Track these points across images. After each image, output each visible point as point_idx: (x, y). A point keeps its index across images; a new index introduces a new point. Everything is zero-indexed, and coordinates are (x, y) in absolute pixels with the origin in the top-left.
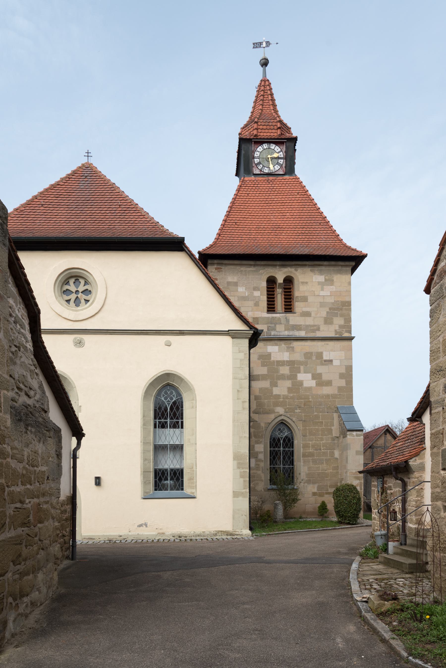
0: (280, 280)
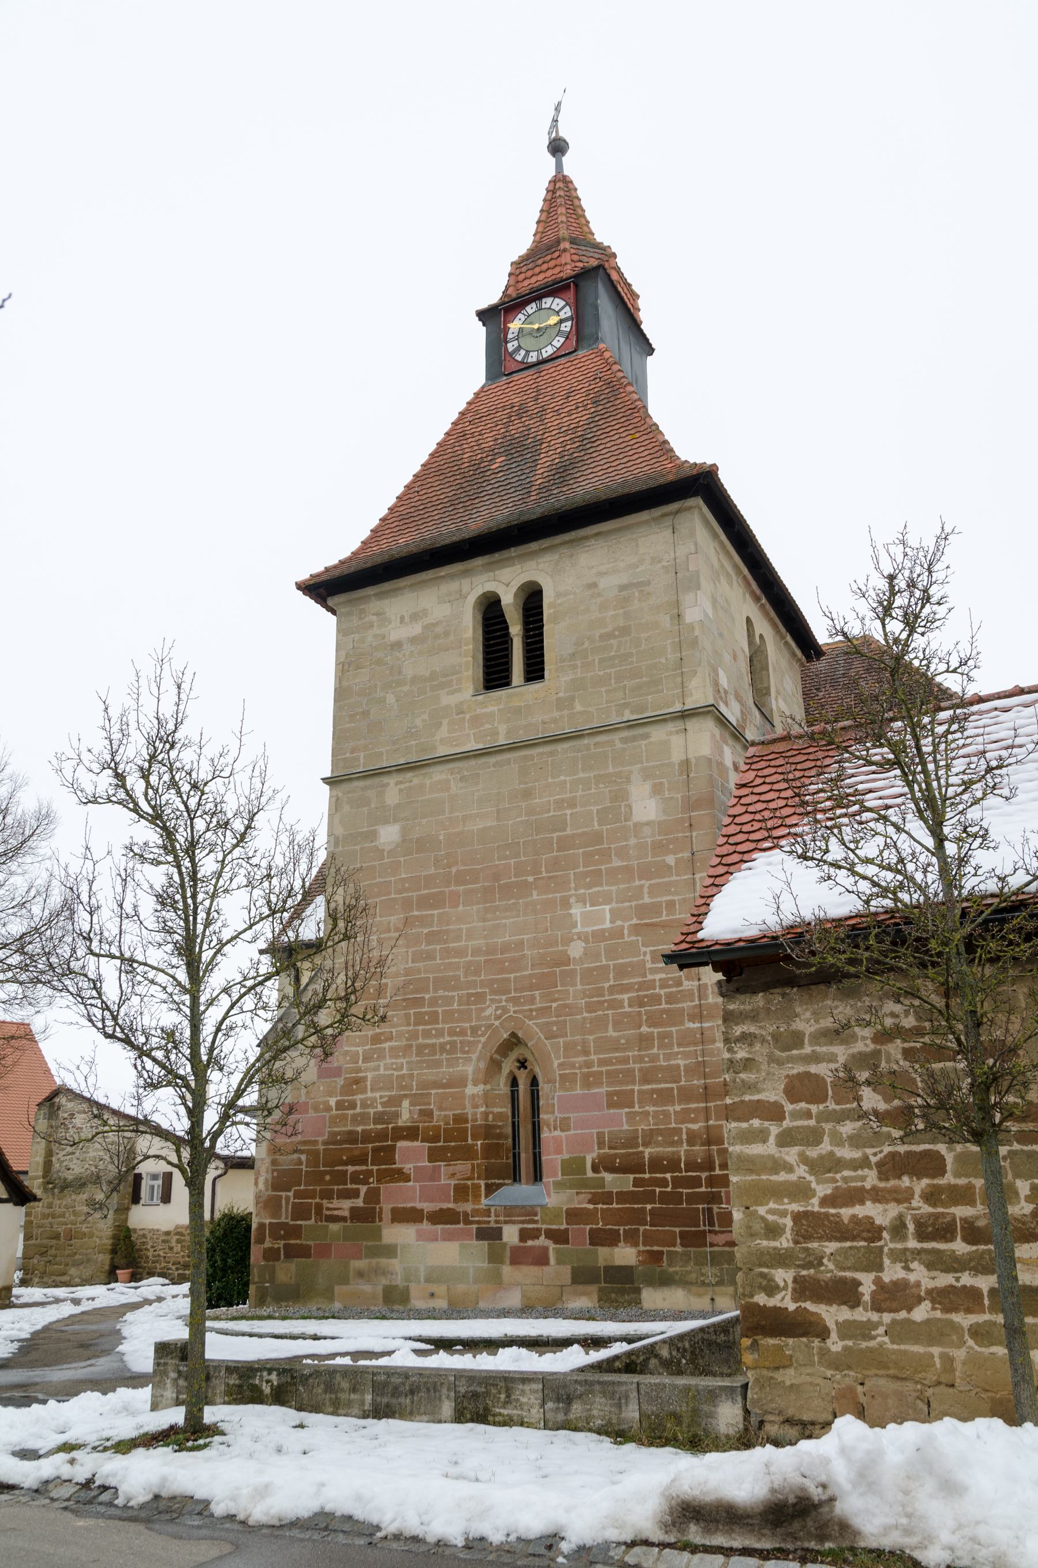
0: (508, 599)
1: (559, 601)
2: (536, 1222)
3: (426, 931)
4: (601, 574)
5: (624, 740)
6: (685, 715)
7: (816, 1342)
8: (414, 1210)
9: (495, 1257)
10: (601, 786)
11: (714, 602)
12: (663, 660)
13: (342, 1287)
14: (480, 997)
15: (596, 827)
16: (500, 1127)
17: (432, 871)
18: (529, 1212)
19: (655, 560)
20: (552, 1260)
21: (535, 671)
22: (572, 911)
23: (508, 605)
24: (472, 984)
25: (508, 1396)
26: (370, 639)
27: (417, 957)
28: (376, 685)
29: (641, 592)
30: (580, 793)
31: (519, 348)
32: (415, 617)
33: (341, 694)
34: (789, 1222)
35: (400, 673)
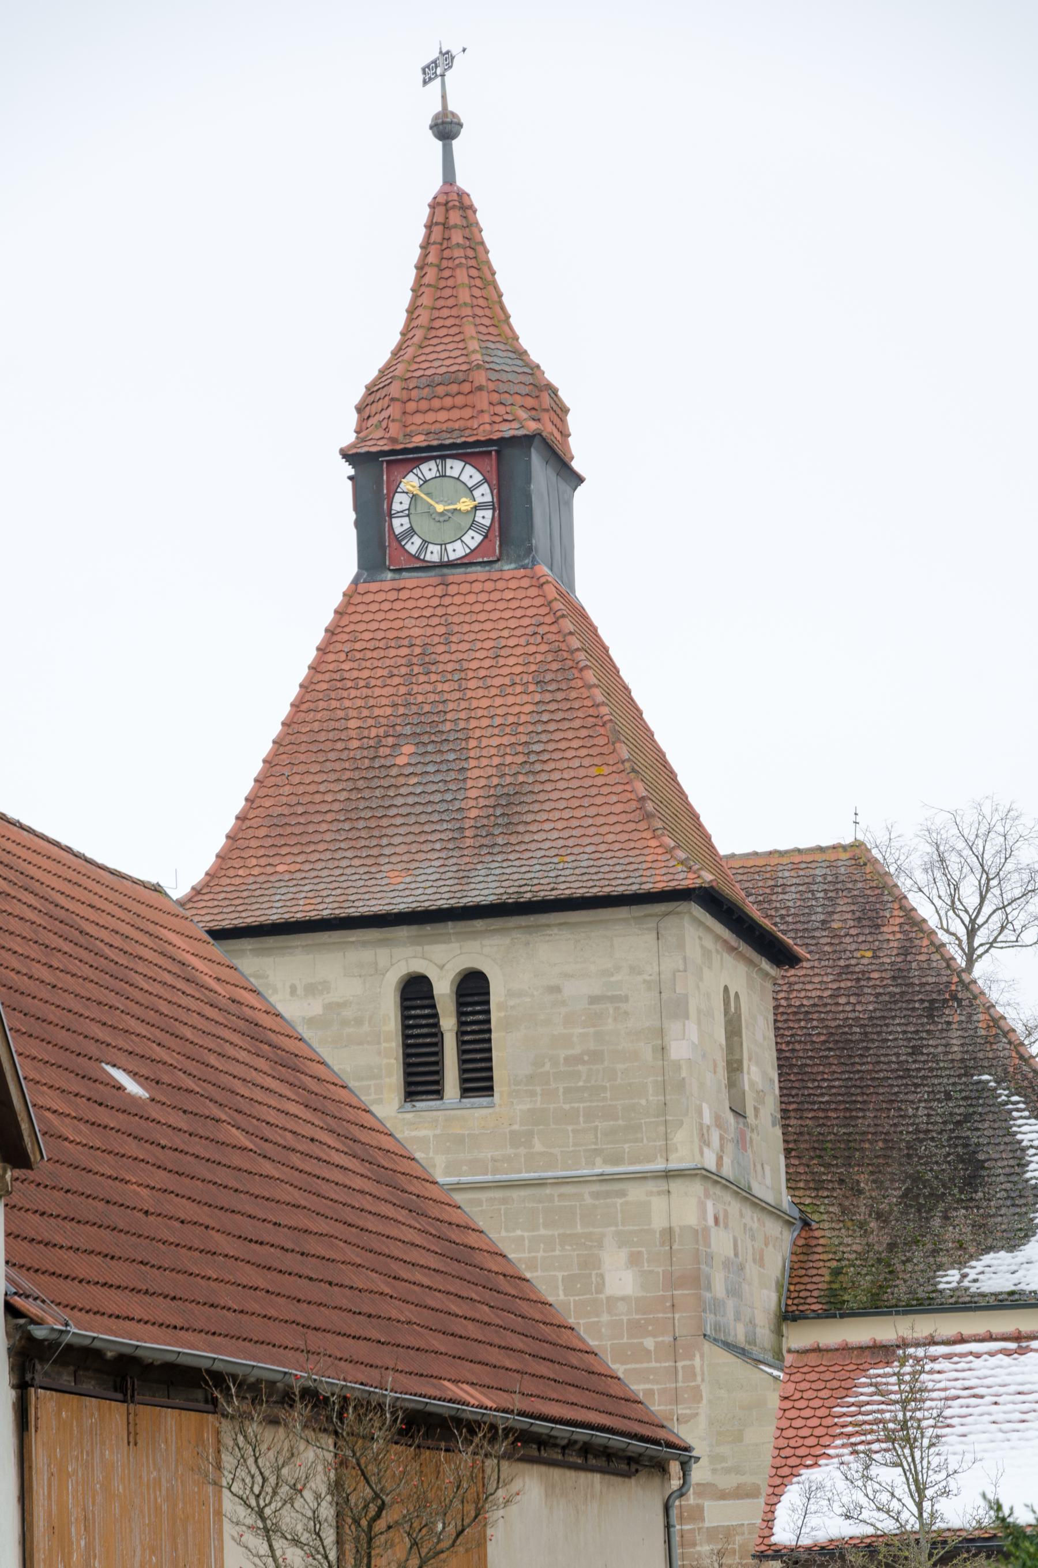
0: (443, 988)
1: (511, 1003)
4: (567, 976)
5: (596, 1195)
6: (668, 1175)
10: (568, 1247)
15: (562, 1297)
23: (443, 995)
29: (617, 1009)
30: (540, 1254)
31: (411, 531)
32: (312, 990)
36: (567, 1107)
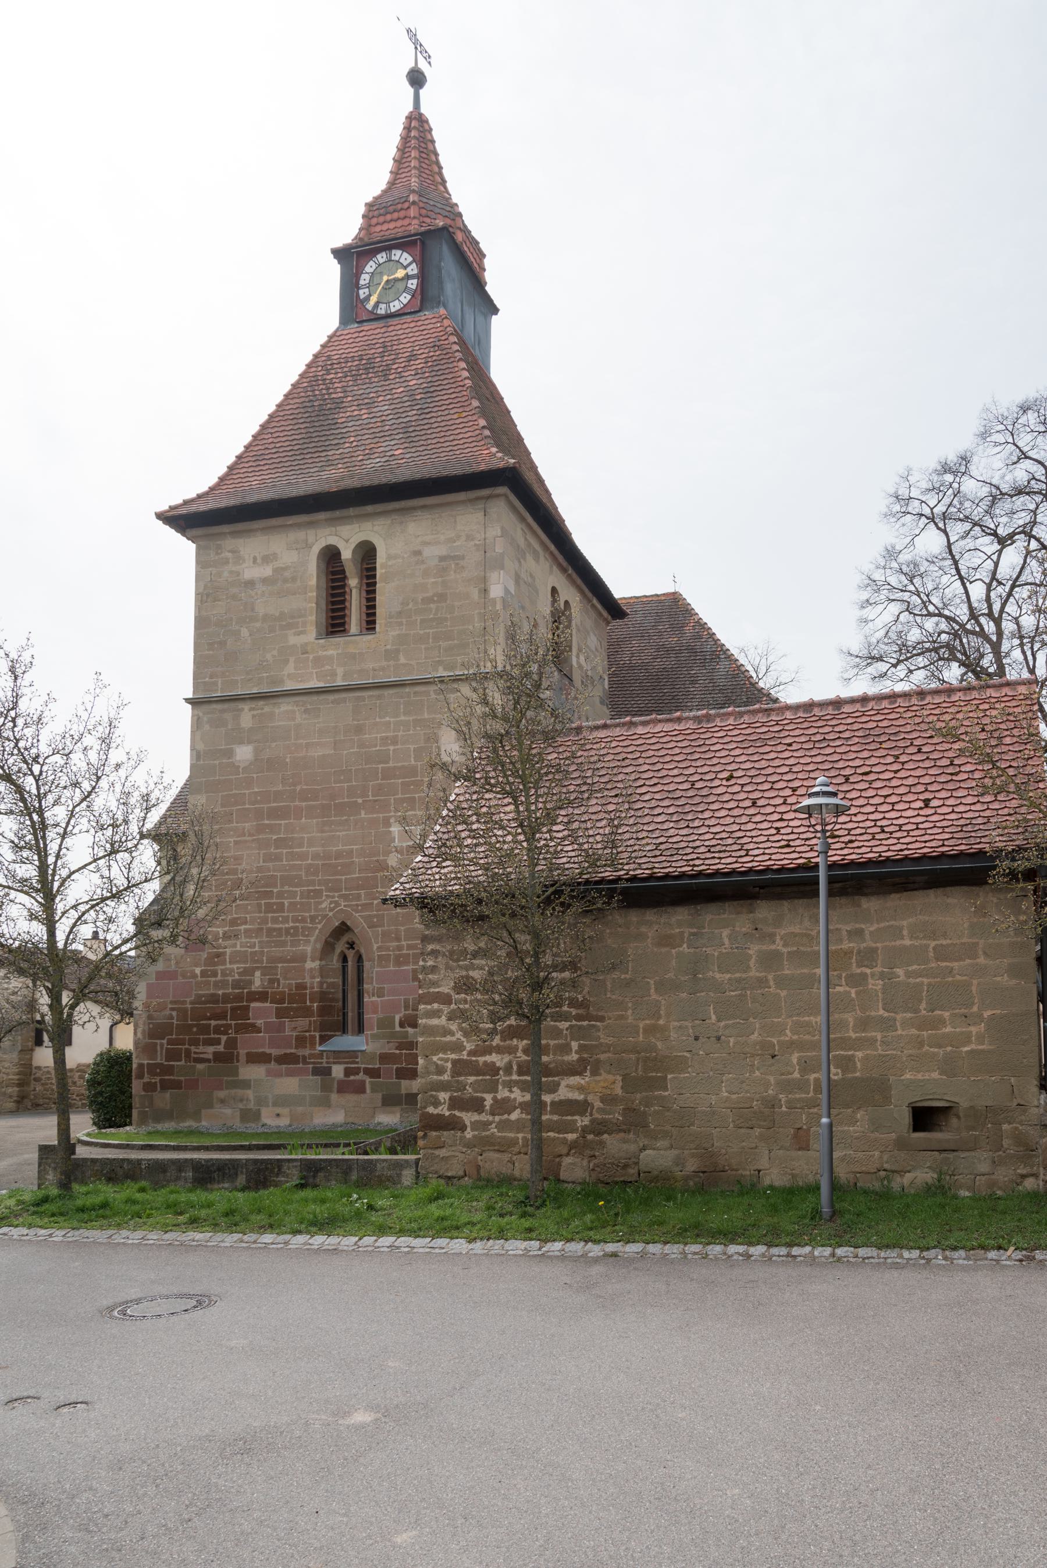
0: (346, 554)
1: (390, 563)
2: (357, 1063)
3: (275, 837)
7: (459, 1134)
8: (264, 1054)
9: (326, 1088)
11: (517, 579)
12: (471, 627)
13: (209, 1110)
14: (318, 893)
15: (413, 762)
16: (333, 993)
17: (280, 788)
18: (352, 1055)
19: (469, 538)
20: (368, 1090)
21: (370, 624)
22: (392, 829)
24: (312, 883)
25: (279, 1170)
26: (226, 574)
27: (268, 858)
28: (231, 619)
30: (401, 733)
32: (266, 559)
33: (201, 622)
34: (449, 1065)
35: (253, 610)
36: (422, 632)
